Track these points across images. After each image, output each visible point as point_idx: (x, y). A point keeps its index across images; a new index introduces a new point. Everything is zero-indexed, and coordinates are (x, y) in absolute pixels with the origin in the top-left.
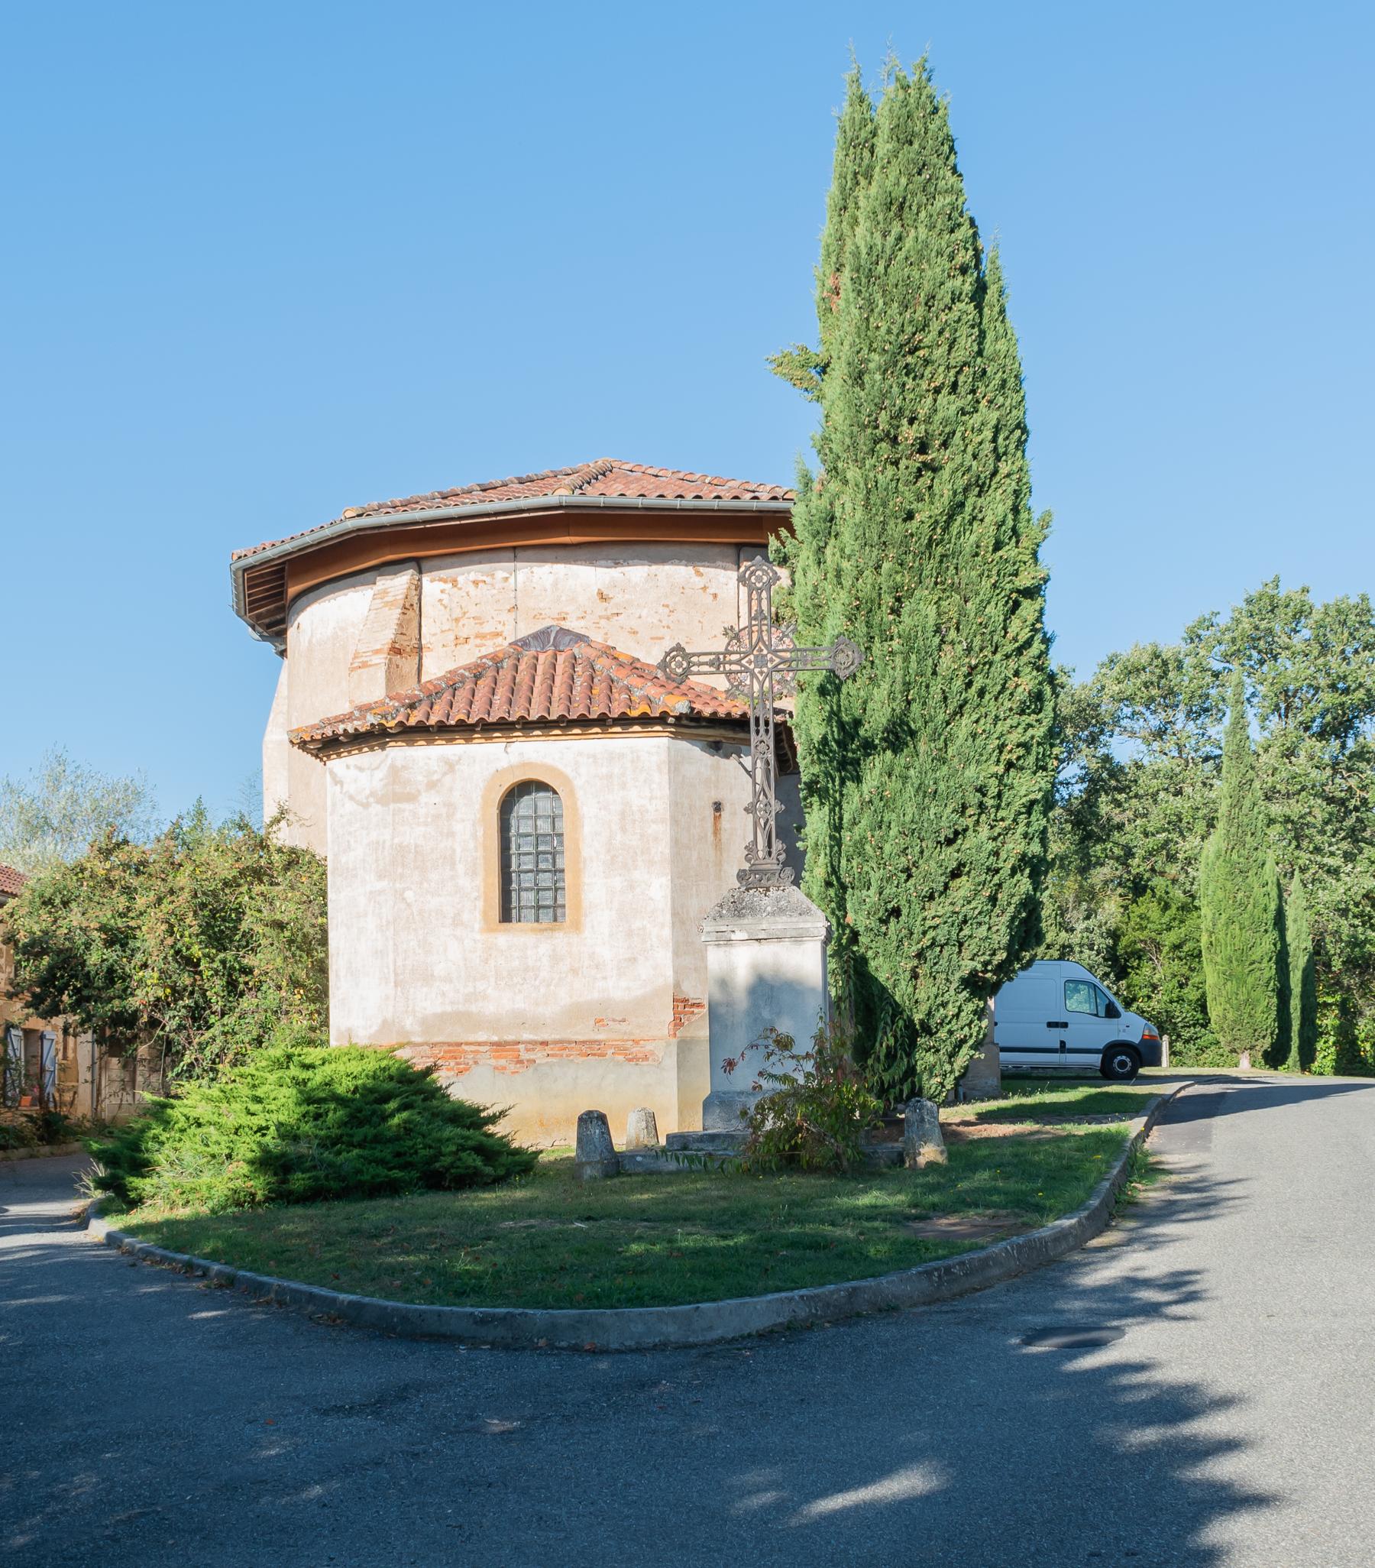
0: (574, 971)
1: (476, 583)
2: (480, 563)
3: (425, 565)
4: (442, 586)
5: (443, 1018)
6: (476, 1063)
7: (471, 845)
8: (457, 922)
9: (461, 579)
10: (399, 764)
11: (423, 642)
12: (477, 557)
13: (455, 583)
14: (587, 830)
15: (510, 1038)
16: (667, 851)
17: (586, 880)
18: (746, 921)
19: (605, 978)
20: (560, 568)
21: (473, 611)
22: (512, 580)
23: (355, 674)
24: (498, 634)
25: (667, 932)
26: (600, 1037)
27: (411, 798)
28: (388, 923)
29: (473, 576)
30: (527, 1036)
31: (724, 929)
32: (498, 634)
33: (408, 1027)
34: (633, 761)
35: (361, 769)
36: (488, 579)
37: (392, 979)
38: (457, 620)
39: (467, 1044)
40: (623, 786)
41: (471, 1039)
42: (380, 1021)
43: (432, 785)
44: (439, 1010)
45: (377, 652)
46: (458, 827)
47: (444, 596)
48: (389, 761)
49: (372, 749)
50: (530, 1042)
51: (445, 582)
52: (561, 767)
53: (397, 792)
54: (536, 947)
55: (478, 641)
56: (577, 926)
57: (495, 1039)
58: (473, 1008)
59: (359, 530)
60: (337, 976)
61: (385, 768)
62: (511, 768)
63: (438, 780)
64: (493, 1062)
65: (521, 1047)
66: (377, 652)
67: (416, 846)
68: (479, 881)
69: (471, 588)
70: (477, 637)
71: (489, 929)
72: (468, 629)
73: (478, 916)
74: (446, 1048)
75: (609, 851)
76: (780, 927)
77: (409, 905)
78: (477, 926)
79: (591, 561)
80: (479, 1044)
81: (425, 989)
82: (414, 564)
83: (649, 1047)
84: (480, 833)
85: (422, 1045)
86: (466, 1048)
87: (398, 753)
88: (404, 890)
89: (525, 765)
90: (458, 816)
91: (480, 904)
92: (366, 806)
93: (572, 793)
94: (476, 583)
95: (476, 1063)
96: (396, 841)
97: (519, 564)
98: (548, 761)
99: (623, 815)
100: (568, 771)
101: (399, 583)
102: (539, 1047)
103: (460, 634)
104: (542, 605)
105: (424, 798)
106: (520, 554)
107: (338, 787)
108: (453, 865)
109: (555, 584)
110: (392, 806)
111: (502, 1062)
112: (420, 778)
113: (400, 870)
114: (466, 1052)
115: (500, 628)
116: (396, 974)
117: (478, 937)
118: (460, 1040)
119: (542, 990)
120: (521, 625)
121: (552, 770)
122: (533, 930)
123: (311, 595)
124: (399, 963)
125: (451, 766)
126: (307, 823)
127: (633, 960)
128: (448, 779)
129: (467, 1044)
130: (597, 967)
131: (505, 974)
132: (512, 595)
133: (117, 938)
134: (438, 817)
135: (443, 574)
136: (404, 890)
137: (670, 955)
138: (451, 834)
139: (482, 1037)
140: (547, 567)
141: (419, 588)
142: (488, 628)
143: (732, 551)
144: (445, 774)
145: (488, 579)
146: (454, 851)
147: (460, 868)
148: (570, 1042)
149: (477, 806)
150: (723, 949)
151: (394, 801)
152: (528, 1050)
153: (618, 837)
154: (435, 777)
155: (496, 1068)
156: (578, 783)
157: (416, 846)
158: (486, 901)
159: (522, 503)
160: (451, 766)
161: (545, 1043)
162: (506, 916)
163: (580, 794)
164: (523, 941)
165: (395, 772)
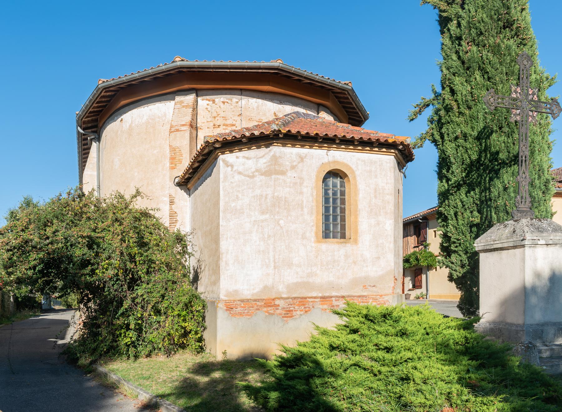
0: (355, 263)
1: (224, 103)
2: (226, 94)
3: (199, 93)
4: (208, 102)
5: (297, 285)
6: (313, 307)
7: (311, 199)
8: (304, 237)
9: (217, 100)
10: (278, 155)
11: (198, 125)
12: (225, 92)
13: (214, 101)
14: (361, 196)
15: (327, 294)
16: (393, 208)
17: (360, 220)
18: (544, 235)
19: (367, 266)
20: (260, 101)
21: (222, 114)
22: (240, 103)
23: (173, 134)
24: (233, 125)
25: (392, 245)
26: (365, 294)
27: (283, 173)
28: (269, 236)
29: (222, 99)
30: (334, 294)
31: (535, 238)
32: (233, 125)
33: (280, 290)
34: (380, 166)
35: (248, 158)
36: (229, 102)
37: (272, 264)
38: (215, 117)
39: (309, 298)
40: (376, 177)
41: (310, 295)
42: (261, 286)
43: (293, 168)
44: (295, 281)
45: (183, 125)
46: (305, 190)
47: (208, 107)
48: (272, 153)
49: (259, 147)
50: (337, 297)
51: (209, 101)
52: (350, 164)
53: (274, 170)
54: (339, 251)
55: (224, 127)
56: (356, 242)
57: (320, 295)
58: (311, 280)
59: (181, 68)
60: (227, 264)
61: (268, 158)
62: (329, 163)
63: (296, 165)
64: (321, 306)
65: (333, 299)
66: (183, 125)
67: (285, 198)
68: (314, 217)
69: (222, 104)
70: (224, 125)
71: (318, 241)
72: (219, 121)
73: (313, 234)
74: (300, 300)
75: (369, 206)
76: (558, 238)
77: (281, 227)
78: (313, 239)
79: (272, 100)
80: (315, 298)
81: (289, 270)
82: (195, 91)
83: (386, 298)
84: (315, 194)
85: (288, 298)
86: (308, 299)
87: (276, 149)
88: (279, 220)
89: (335, 162)
90: (305, 184)
91: (314, 228)
92: (253, 177)
93: (355, 178)
94: (224, 103)
95: (313, 307)
96: (276, 194)
97: (243, 97)
98: (345, 161)
99: (375, 190)
100: (353, 167)
101: (191, 98)
102: (341, 299)
103: (216, 123)
104: (252, 115)
105: (289, 174)
106: (244, 93)
107: (229, 168)
108: (302, 210)
109: (258, 107)
110: (273, 177)
111: (325, 307)
112: (288, 163)
113: (277, 210)
114: (308, 301)
115: (234, 123)
116: (275, 263)
117: (313, 245)
118: (304, 296)
119: (341, 271)
120: (243, 122)
121: (347, 166)
122: (337, 243)
123: (127, 108)
124: (277, 257)
125: (302, 159)
126: (150, 198)
127: (378, 258)
128: (300, 165)
129: (309, 298)
130: (364, 261)
131: (325, 263)
132: (240, 109)
133: (92, 243)
134: (295, 184)
135: (208, 97)
136: (279, 220)
137: (393, 256)
138: (301, 193)
139: (314, 294)
140: (255, 100)
141: (197, 101)
142: (229, 122)
143: (316, 106)
144: (299, 163)
145: (229, 102)
146: (303, 201)
147: (306, 210)
148: (354, 296)
149: (314, 180)
150: (532, 249)
151: (275, 174)
152: (336, 300)
153: (373, 201)
154: (295, 164)
155: (323, 309)
156: (357, 173)
157: (285, 198)
158: (317, 227)
159: (257, 64)
160: (302, 159)
161: (343, 297)
162: (326, 235)
163: (358, 178)
164: (332, 247)
165: (275, 159)
